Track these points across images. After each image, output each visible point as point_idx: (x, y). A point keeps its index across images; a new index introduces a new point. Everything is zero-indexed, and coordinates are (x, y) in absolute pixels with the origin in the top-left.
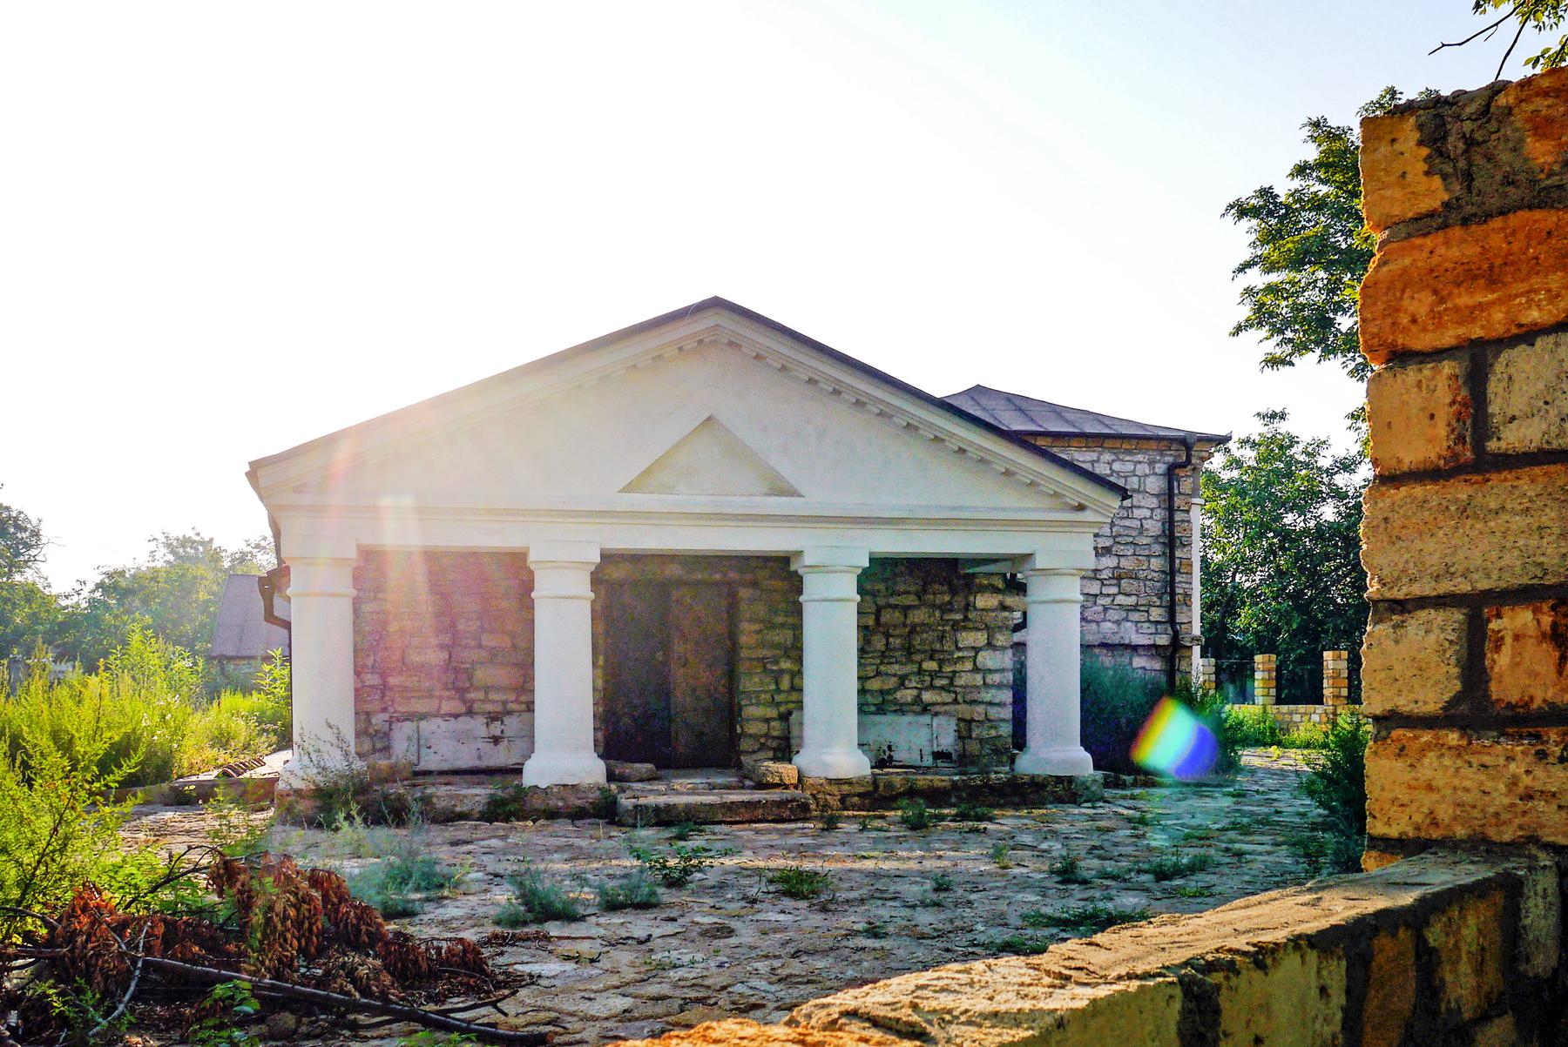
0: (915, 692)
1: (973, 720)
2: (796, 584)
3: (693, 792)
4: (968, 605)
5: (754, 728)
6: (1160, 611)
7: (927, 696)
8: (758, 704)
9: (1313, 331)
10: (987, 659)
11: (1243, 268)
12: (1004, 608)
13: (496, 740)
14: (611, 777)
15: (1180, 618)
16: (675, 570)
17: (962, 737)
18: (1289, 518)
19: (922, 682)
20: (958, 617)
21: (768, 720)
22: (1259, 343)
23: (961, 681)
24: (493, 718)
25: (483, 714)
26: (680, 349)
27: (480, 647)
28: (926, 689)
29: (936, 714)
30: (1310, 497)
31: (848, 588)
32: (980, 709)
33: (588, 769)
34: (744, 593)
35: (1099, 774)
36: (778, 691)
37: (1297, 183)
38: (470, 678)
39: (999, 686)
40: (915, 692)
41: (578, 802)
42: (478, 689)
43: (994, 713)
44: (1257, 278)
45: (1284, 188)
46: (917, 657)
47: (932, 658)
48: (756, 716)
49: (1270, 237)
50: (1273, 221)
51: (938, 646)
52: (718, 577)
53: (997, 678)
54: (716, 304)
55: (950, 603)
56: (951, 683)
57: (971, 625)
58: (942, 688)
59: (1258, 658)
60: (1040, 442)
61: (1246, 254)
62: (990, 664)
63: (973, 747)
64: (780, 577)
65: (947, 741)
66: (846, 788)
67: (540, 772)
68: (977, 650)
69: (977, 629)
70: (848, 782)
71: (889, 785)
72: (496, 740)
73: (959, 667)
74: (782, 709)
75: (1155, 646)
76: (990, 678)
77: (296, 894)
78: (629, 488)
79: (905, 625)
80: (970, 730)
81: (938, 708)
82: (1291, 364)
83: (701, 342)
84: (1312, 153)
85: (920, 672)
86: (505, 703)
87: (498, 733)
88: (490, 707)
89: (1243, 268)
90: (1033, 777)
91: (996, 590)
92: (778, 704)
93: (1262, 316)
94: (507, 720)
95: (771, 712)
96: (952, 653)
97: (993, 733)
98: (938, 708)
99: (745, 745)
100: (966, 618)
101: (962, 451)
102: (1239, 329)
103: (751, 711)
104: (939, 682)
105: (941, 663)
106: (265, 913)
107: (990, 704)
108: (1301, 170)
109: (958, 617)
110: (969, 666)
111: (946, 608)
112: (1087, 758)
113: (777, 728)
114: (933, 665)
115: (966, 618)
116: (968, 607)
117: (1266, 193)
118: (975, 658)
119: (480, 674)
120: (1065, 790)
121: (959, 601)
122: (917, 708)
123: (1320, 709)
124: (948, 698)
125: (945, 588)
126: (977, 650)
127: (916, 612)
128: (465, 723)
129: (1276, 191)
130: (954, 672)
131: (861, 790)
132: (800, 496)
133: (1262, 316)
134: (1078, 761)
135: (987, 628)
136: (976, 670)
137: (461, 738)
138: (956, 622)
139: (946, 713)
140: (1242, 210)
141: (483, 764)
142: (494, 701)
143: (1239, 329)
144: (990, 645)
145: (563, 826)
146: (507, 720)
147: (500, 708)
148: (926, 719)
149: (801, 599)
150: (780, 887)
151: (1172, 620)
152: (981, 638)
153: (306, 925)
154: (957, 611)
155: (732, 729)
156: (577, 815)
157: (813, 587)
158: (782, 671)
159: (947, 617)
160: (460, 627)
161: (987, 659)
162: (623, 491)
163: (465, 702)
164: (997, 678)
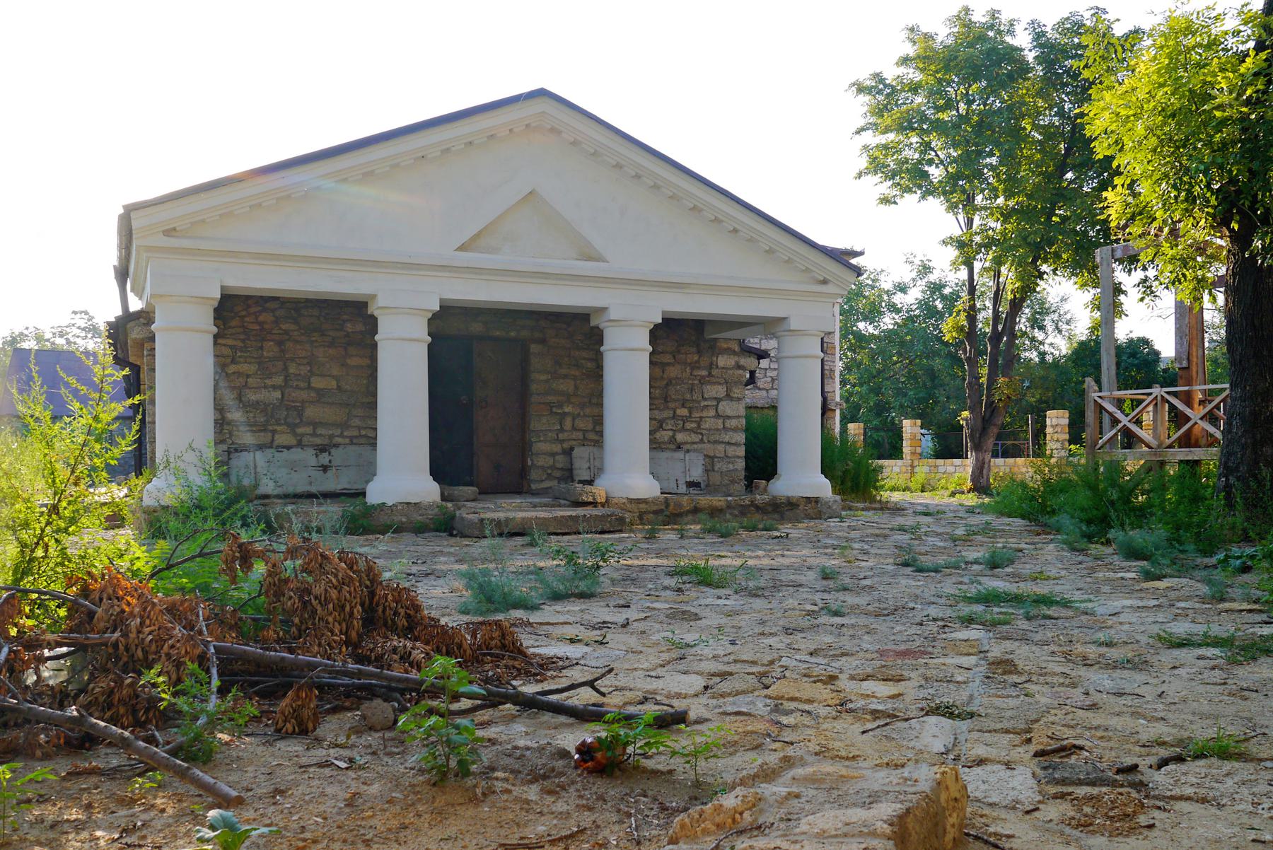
0: (671, 433)
1: (715, 457)
2: (597, 337)
3: (520, 509)
4: (711, 364)
5: (542, 461)
7: (680, 437)
8: (545, 441)
9: (912, 178)
10: (726, 408)
11: (858, 132)
12: (739, 367)
13: (325, 468)
14: (443, 498)
16: (476, 328)
17: (708, 470)
18: (861, 325)
19: (676, 425)
20: (704, 373)
21: (553, 455)
22: (877, 186)
23: (706, 425)
24: (322, 449)
25: (312, 446)
26: (511, 130)
28: (680, 431)
29: (688, 451)
30: (873, 314)
31: (642, 340)
32: (721, 447)
33: (426, 490)
34: (534, 348)
35: (838, 498)
36: (562, 430)
37: (901, 70)
38: (300, 416)
39: (735, 430)
40: (671, 433)
41: (420, 518)
43: (731, 451)
44: (871, 139)
45: (891, 73)
46: (672, 405)
47: (683, 406)
48: (544, 451)
49: (880, 111)
50: (881, 98)
51: (688, 396)
52: (513, 334)
53: (734, 423)
54: (541, 93)
55: (697, 362)
56: (699, 426)
58: (692, 430)
61: (862, 122)
62: (729, 413)
63: (715, 478)
64: (578, 334)
65: (697, 474)
66: (643, 506)
67: (381, 491)
68: (719, 400)
69: (720, 384)
70: (644, 501)
71: (679, 505)
72: (325, 468)
73: (704, 414)
74: (566, 445)
76: (729, 423)
77: (336, 576)
78: (462, 248)
79: (662, 378)
81: (688, 447)
82: (895, 203)
83: (527, 126)
84: (910, 50)
85: (674, 417)
86: (331, 437)
87: (326, 462)
88: (318, 441)
89: (858, 132)
90: (788, 498)
91: (734, 353)
92: (562, 441)
93: (876, 166)
94: (333, 451)
95: (557, 448)
96: (699, 402)
97: (731, 467)
98: (688, 447)
99: (534, 475)
100: (710, 375)
101: (735, 231)
102: (860, 175)
103: (541, 447)
104: (689, 426)
105: (690, 410)
106: (301, 598)
107: (729, 443)
108: (905, 61)
109: (704, 373)
110: (712, 413)
111: (695, 366)
112: (826, 483)
113: (561, 461)
114: (684, 412)
115: (710, 375)
116: (711, 366)
117: (878, 77)
119: (311, 412)
120: (810, 508)
121: (705, 361)
122: (673, 446)
123: (899, 462)
124: (696, 438)
125: (694, 349)
126: (719, 400)
127: (671, 368)
128: (297, 454)
129: (885, 76)
131: (655, 508)
132: (605, 261)
133: (876, 166)
134: (822, 487)
136: (718, 416)
137: (293, 467)
138: (703, 377)
139: (695, 450)
140: (861, 89)
141: (314, 489)
142: (321, 435)
143: (860, 175)
144: (728, 397)
145: (408, 537)
146: (333, 451)
147: (326, 442)
148: (680, 455)
149: (602, 349)
150: (694, 578)
152: (720, 391)
153: (348, 608)
155: (524, 462)
156: (420, 529)
157: (614, 340)
158: (565, 414)
159: (695, 373)
160: (291, 371)
161: (726, 408)
163: (295, 434)
164: (734, 423)
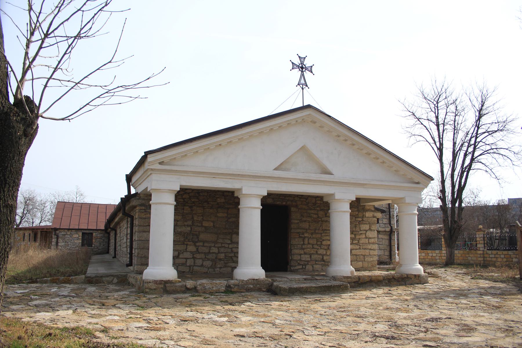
6: (386, 220)
8: (297, 249)
12: (374, 217)
15: (392, 223)
20: (360, 219)
27: (202, 226)
32: (368, 251)
36: (304, 244)
38: (198, 238)
42: (201, 241)
43: (372, 252)
57: (364, 222)
58: (356, 244)
59: (499, 231)
60: (27, 63)
62: (371, 236)
68: (366, 231)
73: (361, 237)
75: (385, 231)
78: (276, 169)
80: (364, 259)
91: (372, 211)
97: (372, 259)
100: (363, 220)
107: (371, 249)
110: (364, 236)
116: (363, 216)
118: (366, 233)
121: (360, 215)
124: (358, 247)
126: (366, 231)
130: (359, 238)
132: (332, 174)
135: (369, 223)
136: (366, 238)
138: (360, 221)
151: (390, 224)
152: (366, 227)
154: (360, 217)
157: (244, 204)
158: (305, 237)
162: (275, 169)
